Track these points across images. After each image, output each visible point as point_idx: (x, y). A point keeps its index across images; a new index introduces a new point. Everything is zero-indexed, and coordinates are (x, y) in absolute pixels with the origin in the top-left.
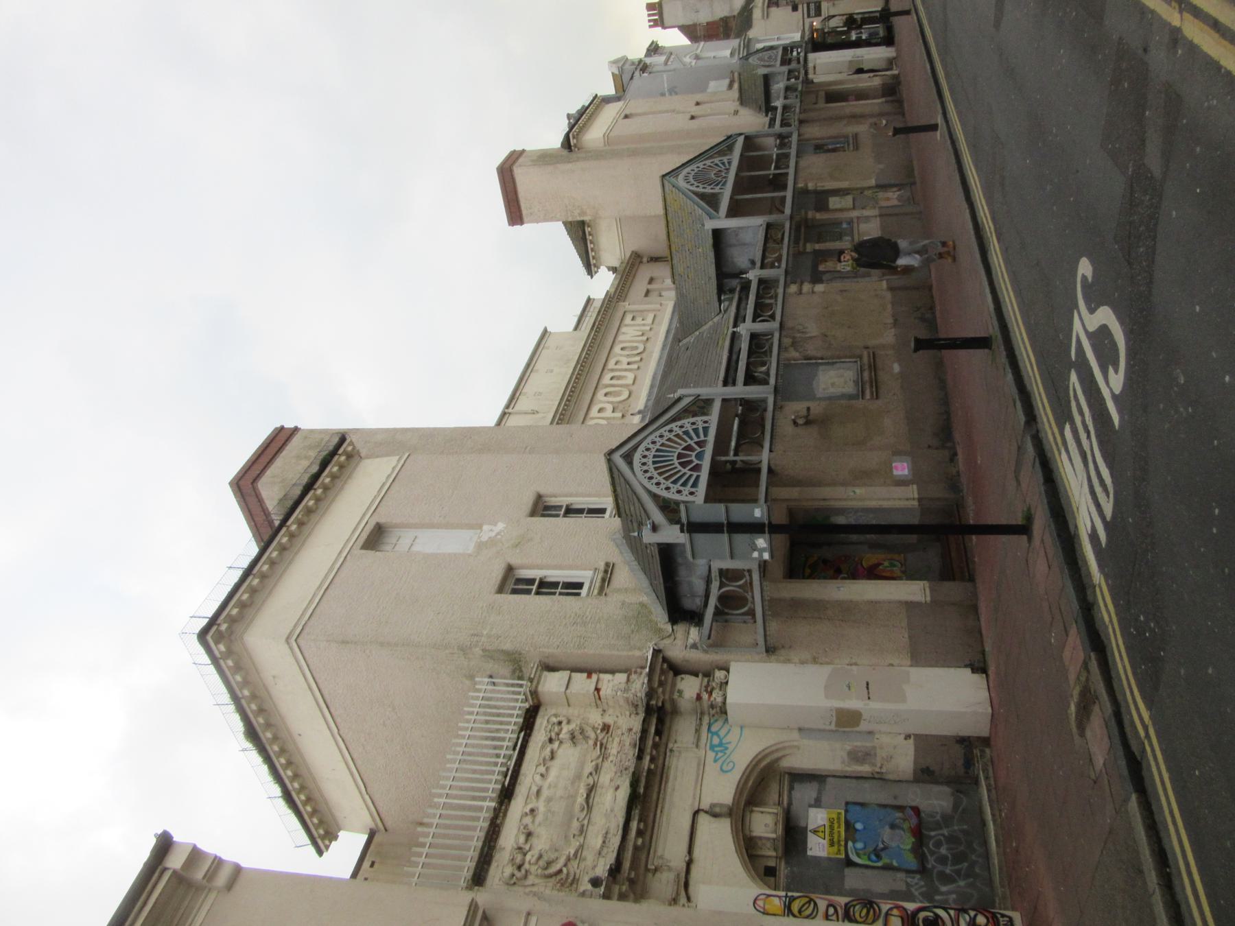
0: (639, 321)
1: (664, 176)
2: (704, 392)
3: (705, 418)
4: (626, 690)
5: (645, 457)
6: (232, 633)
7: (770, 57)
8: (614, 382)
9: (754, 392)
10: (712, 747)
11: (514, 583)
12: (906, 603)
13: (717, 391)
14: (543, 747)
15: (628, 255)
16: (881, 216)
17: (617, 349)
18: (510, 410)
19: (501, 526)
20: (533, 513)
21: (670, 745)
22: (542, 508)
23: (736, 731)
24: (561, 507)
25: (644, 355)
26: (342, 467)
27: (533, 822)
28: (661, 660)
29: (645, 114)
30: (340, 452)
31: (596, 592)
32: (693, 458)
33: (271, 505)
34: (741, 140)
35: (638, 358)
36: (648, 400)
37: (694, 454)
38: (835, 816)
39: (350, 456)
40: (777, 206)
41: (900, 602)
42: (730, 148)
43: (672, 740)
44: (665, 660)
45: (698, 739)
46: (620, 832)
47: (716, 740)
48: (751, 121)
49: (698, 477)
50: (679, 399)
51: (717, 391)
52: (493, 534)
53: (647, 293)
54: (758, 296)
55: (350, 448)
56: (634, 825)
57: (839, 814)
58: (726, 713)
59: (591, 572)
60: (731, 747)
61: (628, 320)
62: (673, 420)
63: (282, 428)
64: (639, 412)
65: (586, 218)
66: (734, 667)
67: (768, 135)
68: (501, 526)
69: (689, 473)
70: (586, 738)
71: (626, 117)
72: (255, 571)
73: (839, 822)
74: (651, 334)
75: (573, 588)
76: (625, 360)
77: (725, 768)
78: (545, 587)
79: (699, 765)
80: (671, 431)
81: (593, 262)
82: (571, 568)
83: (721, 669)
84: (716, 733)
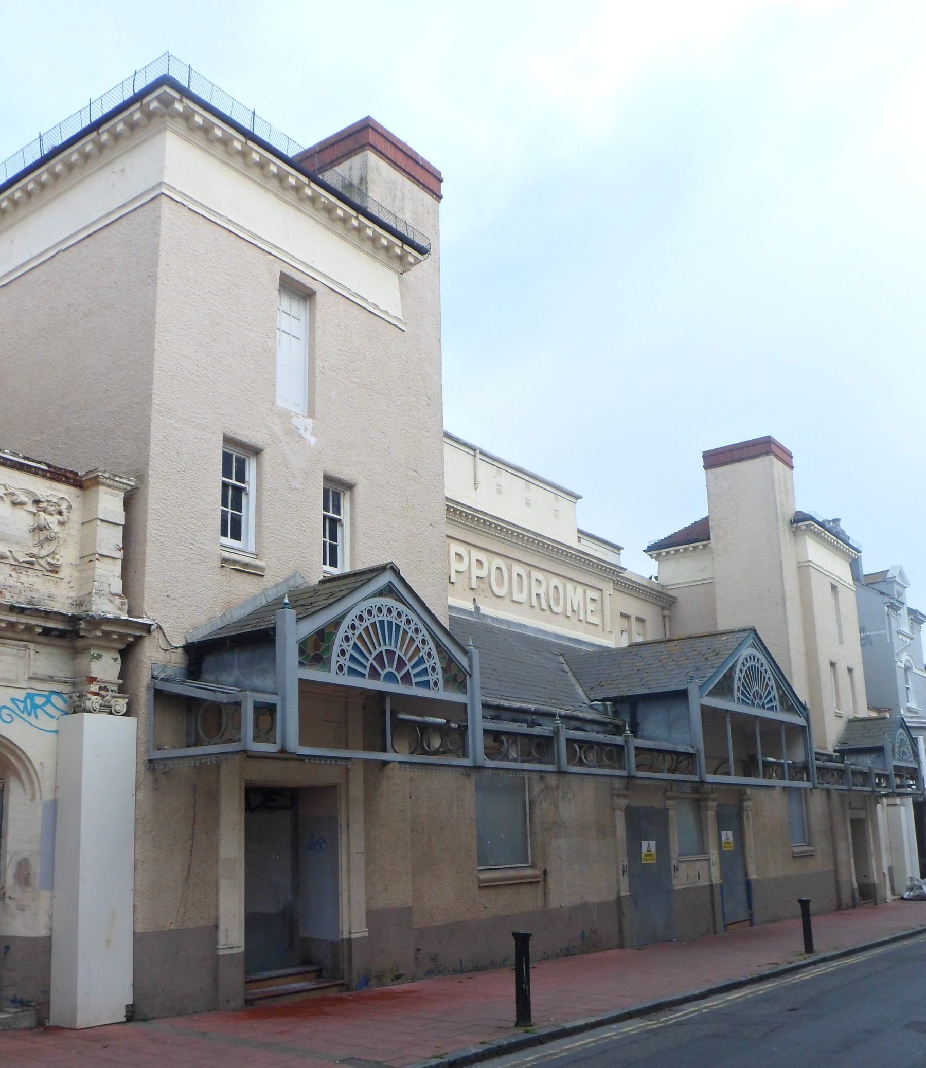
0: (591, 606)
1: (754, 631)
2: (476, 682)
3: (441, 683)
4: (99, 593)
5: (389, 611)
6: (172, 117)
7: (904, 753)
8: (515, 577)
9: (477, 741)
10: (30, 696)
11: (237, 458)
12: (216, 927)
13: (474, 698)
14: (28, 492)
15: (672, 593)
16: (711, 885)
17: (555, 581)
18: (479, 456)
19: (313, 440)
20: (328, 479)
21: (32, 646)
22: (335, 491)
23: (52, 725)
24: (339, 514)
25: (548, 613)
26: (387, 249)
28: (138, 634)
29: (838, 609)
30: (406, 247)
31: (227, 555)
32: (388, 669)
33: (342, 169)
34: (801, 721)
35: (544, 606)
36: (492, 618)
37: (393, 670)
39: (401, 258)
40: (720, 767)
41: (217, 919)
42: (790, 709)
43: (39, 648)
44: (139, 639)
45: (41, 680)
47: (39, 701)
48: (829, 734)
49: (363, 675)
50: (465, 652)
51: (474, 698)
52: (302, 432)
53: (625, 616)
54: (601, 745)
55: (411, 259)
58: (75, 712)
59: (253, 550)
60: (32, 719)
61: (591, 594)
62: (439, 645)
63: (440, 181)
64: (477, 609)
65: (712, 543)
66: (131, 721)
67: (807, 754)
68: (313, 440)
69: (368, 666)
70: (41, 544)
71: (834, 587)
72: (250, 144)
74: (574, 620)
75: (232, 527)
76: (542, 591)
78: (233, 496)
79: (10, 681)
80: (424, 642)
82: (258, 525)
83: (129, 705)
84: (48, 701)
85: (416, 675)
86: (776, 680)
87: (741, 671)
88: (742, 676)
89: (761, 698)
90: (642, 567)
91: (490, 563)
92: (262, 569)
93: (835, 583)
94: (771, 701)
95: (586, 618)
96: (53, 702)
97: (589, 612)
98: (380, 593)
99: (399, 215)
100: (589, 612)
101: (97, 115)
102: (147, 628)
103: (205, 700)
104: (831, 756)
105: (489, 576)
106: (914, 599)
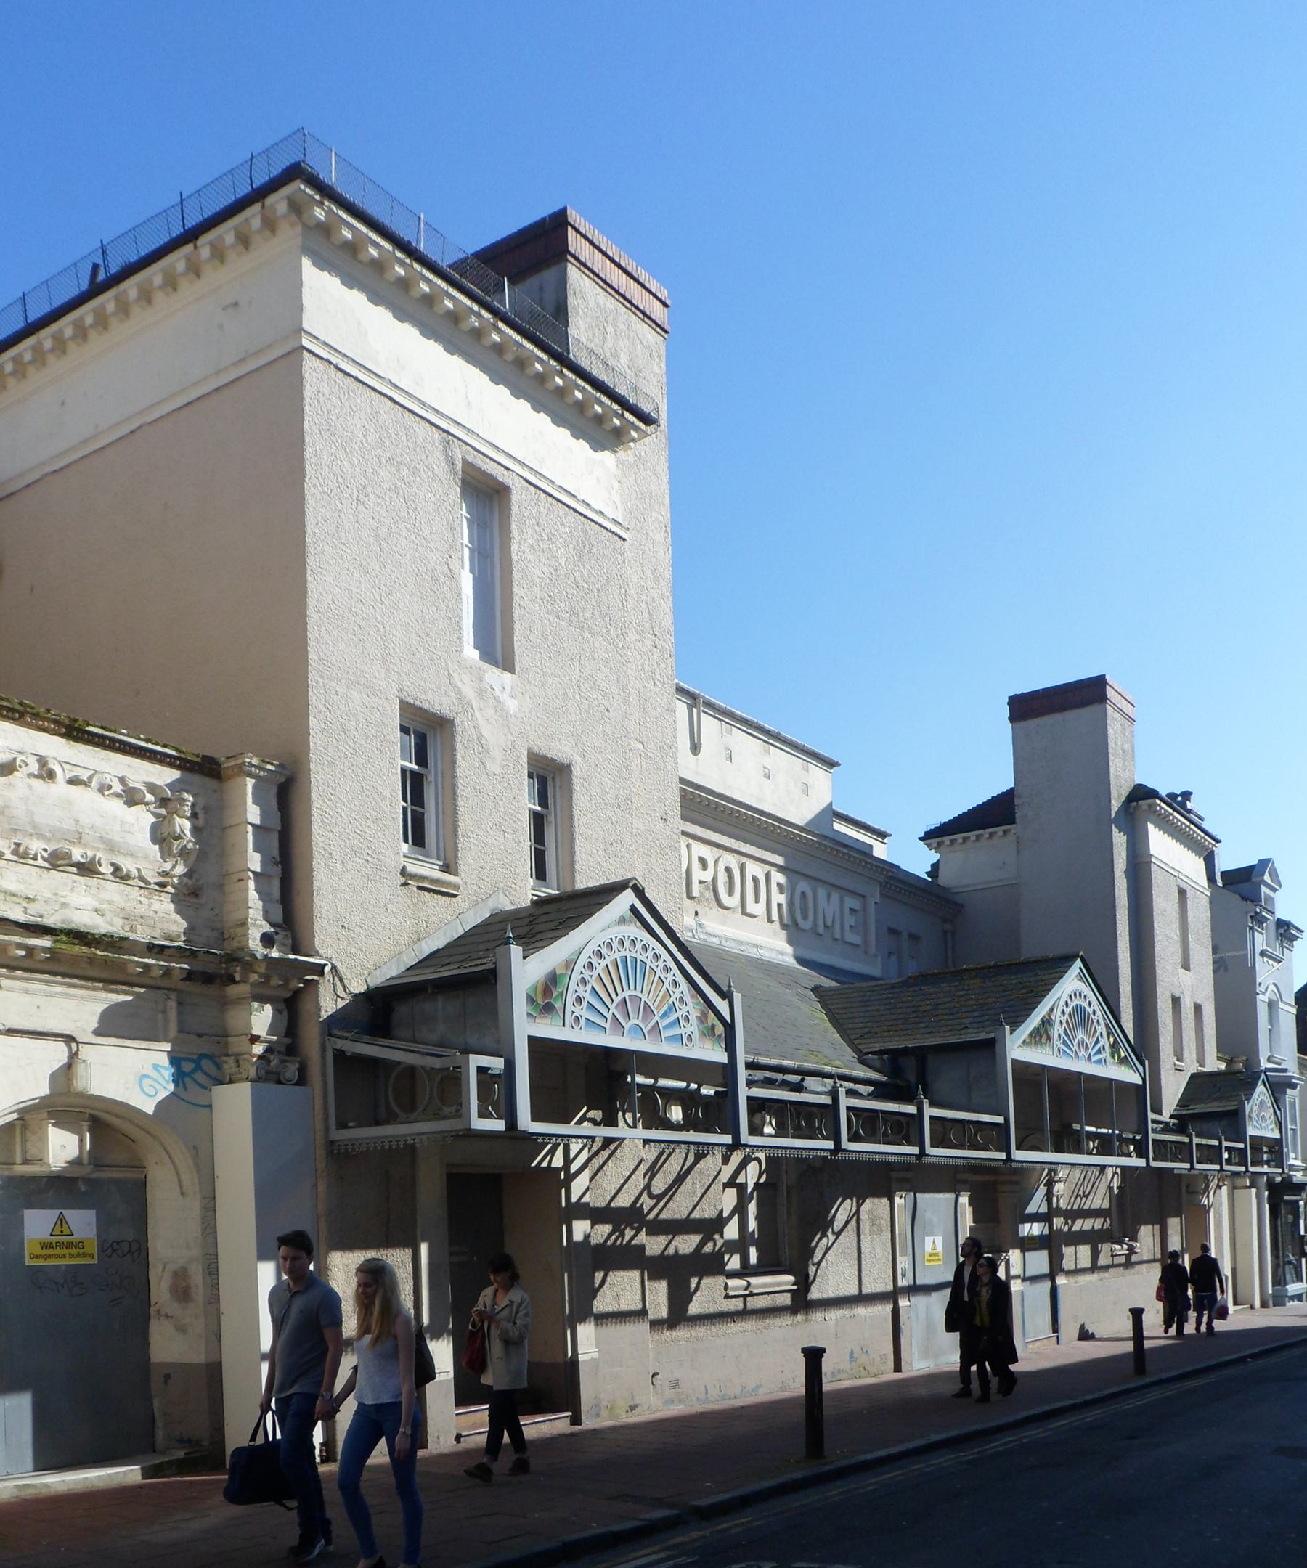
0: (850, 920)
19: (512, 705)
27: (31, 775)
32: (633, 1021)
38: (87, 1250)
46: (33, 920)
52: (498, 693)
56: (46, 942)
57: (92, 1256)
61: (851, 902)
69: (609, 1016)
71: (1182, 893)
73: (78, 1256)
77: (146, 1082)
81: (947, 840)
84: (198, 1067)
85: (666, 1027)
86: (1107, 1026)
87: (1063, 1012)
88: (1064, 1019)
89: (1087, 1047)
90: (917, 860)
91: (716, 862)
92: (456, 887)
93: (1183, 885)
94: (1099, 1052)
95: (842, 935)
96: (205, 1068)
97: (847, 928)
98: (622, 921)
99: (612, 362)
100: (847, 928)
101: (193, 220)
102: (319, 970)
103: (399, 1063)
104: (1167, 1124)
105: (714, 880)
106: (1285, 905)
